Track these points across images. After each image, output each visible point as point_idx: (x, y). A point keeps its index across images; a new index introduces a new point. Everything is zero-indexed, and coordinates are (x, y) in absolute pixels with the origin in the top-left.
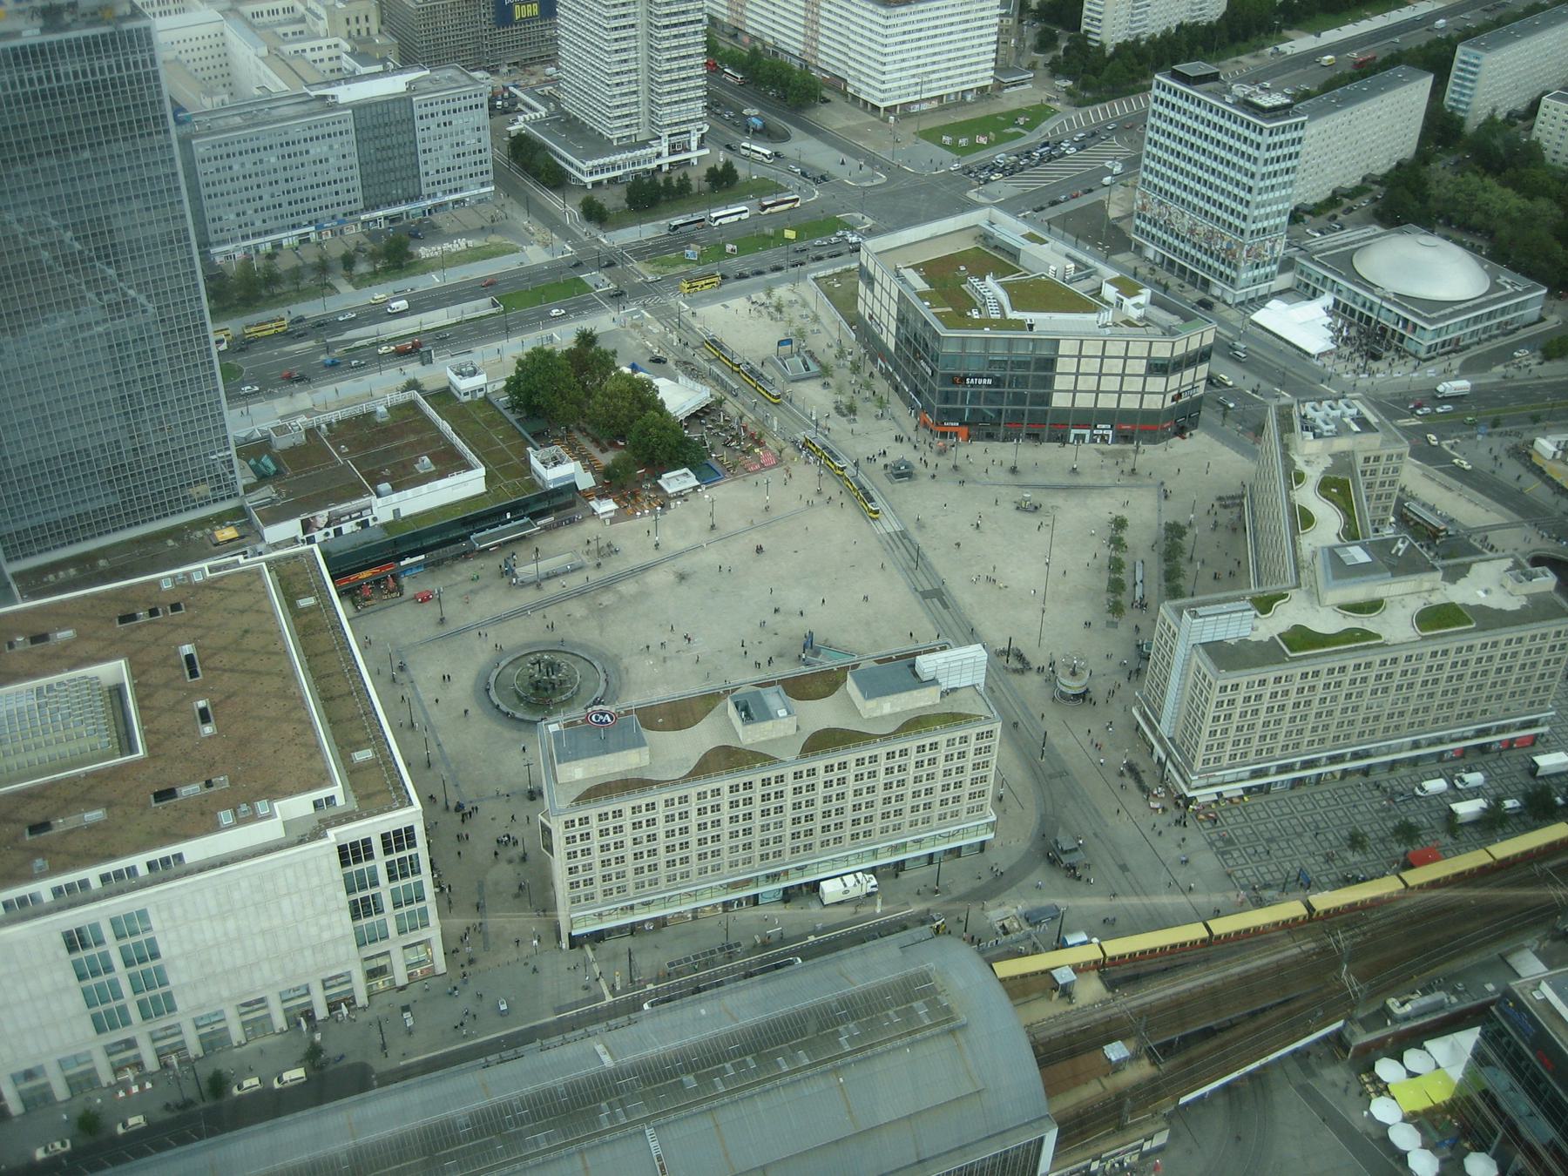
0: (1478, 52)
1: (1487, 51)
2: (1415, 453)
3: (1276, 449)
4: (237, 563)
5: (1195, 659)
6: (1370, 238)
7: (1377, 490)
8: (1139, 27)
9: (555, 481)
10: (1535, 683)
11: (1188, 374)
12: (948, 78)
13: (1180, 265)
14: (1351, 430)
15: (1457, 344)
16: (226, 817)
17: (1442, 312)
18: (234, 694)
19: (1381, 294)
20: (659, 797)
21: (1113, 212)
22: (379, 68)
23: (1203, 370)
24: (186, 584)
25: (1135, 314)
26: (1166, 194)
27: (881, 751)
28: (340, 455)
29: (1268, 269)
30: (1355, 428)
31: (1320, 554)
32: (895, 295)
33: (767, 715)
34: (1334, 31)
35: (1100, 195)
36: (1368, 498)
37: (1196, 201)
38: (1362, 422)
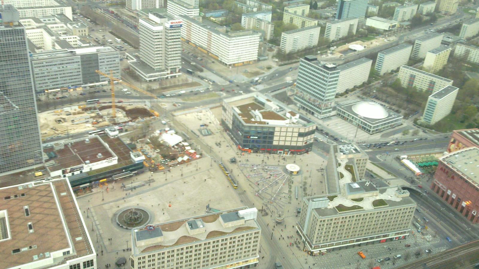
0: (383, 55)
1: (386, 54)
2: (370, 159)
3: (333, 157)
4: (42, 183)
5: (313, 213)
7: (360, 168)
9: (138, 161)
10: (405, 221)
11: (309, 137)
14: (352, 152)
16: (35, 257)
18: (40, 220)
20: (166, 250)
22: (88, 45)
24: (27, 188)
25: (295, 121)
27: (228, 237)
28: (74, 152)
30: (354, 152)
31: (346, 185)
32: (232, 114)
33: (197, 227)
36: (358, 170)
38: (356, 150)
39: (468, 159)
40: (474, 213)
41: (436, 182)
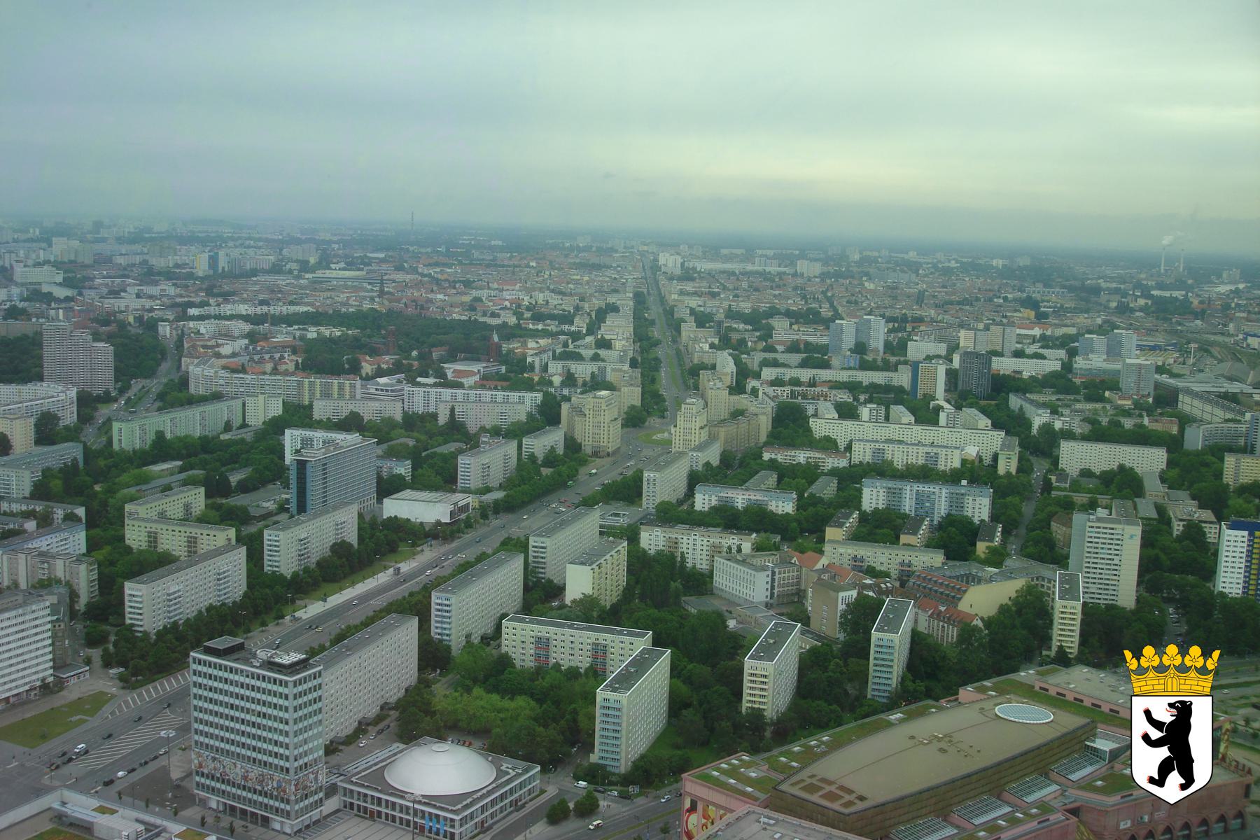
0: (448, 596)
6: (395, 754)
8: (176, 615)
12: (12, 681)
13: (241, 809)
15: (482, 826)
17: (465, 803)
19: (412, 799)
21: (176, 774)
26: (217, 751)
29: (316, 797)
34: (337, 596)
35: (162, 762)
37: (222, 745)
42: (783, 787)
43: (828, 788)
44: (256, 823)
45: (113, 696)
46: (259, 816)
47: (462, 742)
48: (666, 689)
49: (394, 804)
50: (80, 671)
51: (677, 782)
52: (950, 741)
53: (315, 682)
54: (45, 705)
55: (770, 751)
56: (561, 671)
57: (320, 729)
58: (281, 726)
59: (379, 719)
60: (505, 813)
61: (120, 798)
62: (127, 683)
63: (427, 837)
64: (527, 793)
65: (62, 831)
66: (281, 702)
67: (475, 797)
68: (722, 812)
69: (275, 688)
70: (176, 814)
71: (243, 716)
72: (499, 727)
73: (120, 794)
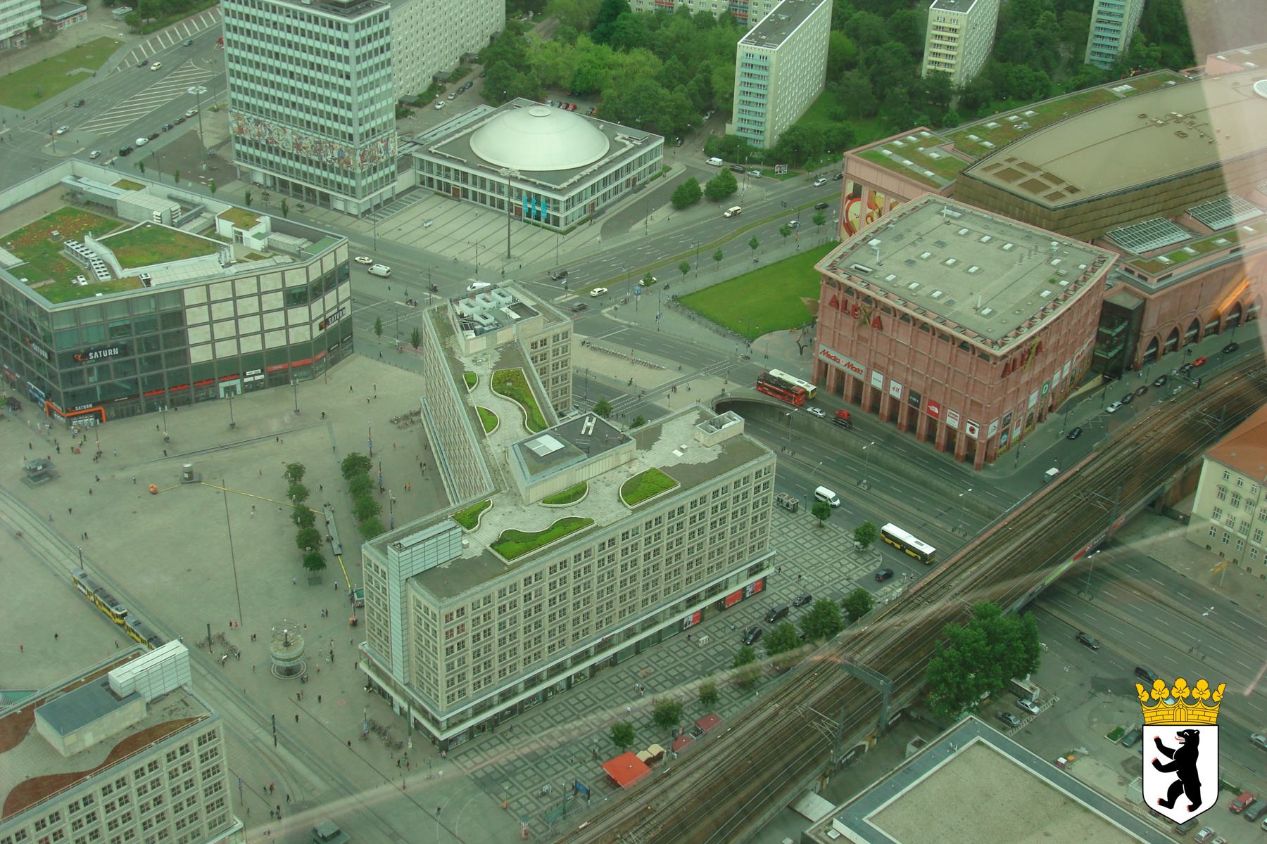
5: (412, 593)
6: (482, 119)
11: (330, 298)
15: (593, 210)
17: (571, 181)
19: (506, 174)
21: (209, 141)
23: (344, 289)
29: (387, 171)
30: (515, 316)
35: (192, 125)
39: (913, 244)
40: (972, 430)
41: (825, 353)
42: (975, 172)
43: (1030, 176)
44: (314, 202)
45: (121, 44)
46: (304, 189)
47: (571, 107)
48: (825, 43)
49: (483, 180)
50: (75, 11)
51: (835, 161)
52: (1192, 123)
53: (381, 26)
54: (35, 56)
55: (954, 126)
56: (690, 18)
57: (390, 85)
58: (341, 82)
59: (457, 75)
60: (620, 194)
61: (143, 171)
62: (138, 27)
63: (525, 221)
64: (647, 171)
65: (79, 212)
66: (339, 50)
67: (584, 173)
68: (892, 200)
69: (331, 32)
70: (214, 190)
71: (291, 68)
72: (611, 87)
73: (142, 166)
